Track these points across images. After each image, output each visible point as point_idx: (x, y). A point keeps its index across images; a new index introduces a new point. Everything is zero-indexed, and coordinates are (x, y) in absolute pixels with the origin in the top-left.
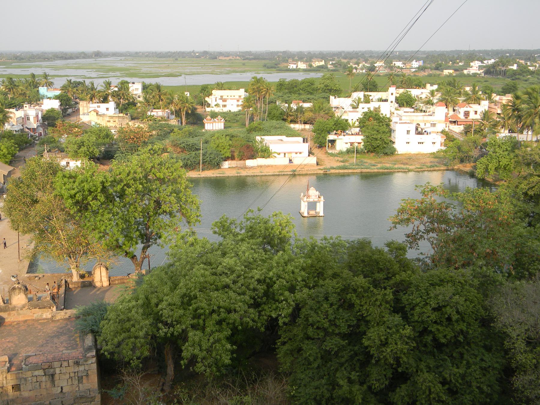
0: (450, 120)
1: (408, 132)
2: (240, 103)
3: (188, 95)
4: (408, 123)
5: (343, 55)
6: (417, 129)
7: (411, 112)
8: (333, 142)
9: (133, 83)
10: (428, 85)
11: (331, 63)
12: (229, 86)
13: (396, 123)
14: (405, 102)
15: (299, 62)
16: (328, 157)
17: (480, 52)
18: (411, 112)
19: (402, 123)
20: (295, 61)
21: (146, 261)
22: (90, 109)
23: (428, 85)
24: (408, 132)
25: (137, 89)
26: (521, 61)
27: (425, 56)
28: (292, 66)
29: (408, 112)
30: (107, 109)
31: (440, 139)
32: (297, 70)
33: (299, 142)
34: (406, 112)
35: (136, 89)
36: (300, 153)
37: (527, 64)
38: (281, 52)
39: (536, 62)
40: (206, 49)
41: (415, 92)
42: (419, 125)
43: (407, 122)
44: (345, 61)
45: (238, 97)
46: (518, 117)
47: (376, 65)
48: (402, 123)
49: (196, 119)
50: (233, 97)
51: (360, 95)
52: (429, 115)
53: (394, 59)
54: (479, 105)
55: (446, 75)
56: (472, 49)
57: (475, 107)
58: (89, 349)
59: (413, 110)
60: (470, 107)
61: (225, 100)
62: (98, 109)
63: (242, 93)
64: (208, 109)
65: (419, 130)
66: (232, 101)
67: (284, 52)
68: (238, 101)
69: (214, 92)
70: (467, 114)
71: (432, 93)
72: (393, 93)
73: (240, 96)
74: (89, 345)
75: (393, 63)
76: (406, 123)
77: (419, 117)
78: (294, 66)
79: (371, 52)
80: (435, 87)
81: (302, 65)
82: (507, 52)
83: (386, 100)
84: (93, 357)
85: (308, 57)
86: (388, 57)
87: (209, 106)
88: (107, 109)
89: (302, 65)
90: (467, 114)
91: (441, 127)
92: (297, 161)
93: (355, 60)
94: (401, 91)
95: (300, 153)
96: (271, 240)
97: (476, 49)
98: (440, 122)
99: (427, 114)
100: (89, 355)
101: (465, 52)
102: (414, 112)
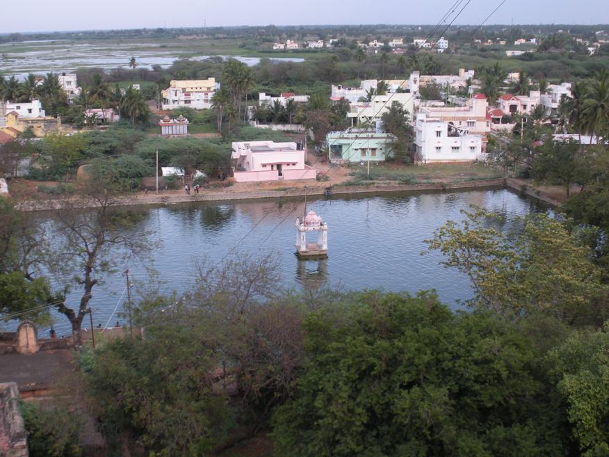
0: (492, 116)
1: (438, 133)
2: (210, 95)
3: (139, 88)
4: (438, 121)
5: (347, 31)
6: (450, 129)
7: (441, 106)
8: (338, 150)
9: (64, 74)
10: (462, 71)
11: (331, 41)
12: (194, 73)
13: (422, 121)
14: (428, 94)
15: (289, 41)
16: (234, 223)
17: (526, 27)
18: (441, 106)
19: (430, 121)
20: (282, 41)
21: (87, 317)
22: (8, 112)
23: (462, 71)
24: (438, 133)
25: (69, 83)
26: (578, 40)
27: (456, 32)
28: (278, 46)
29: (437, 107)
30: (30, 111)
31: (479, 143)
32: (284, 52)
33: (289, 149)
34: (433, 109)
35: (70, 85)
36: (294, 164)
37: (585, 44)
38: (264, 28)
39: (596, 41)
40: (162, 26)
41: (441, 80)
42: (452, 124)
43: (437, 119)
44: (351, 39)
45: (206, 90)
46: (578, 114)
47: (391, 44)
48: (430, 121)
49: (145, 121)
50: (199, 90)
51: (373, 84)
52: (465, 111)
53: (416, 36)
54: (529, 96)
55: (483, 58)
56: (515, 23)
57: (524, 99)
58: (18, 437)
59: (443, 104)
60: (517, 99)
61: (188, 94)
62: (17, 111)
63: (212, 83)
64: (165, 107)
65: (453, 130)
66: (199, 94)
67: (268, 28)
68: (206, 94)
69: (172, 83)
70: (513, 108)
71: (469, 82)
72: (415, 81)
73: (209, 88)
74: (17, 431)
75: (415, 41)
76: (435, 121)
77: (451, 112)
78: (282, 47)
79: (383, 26)
80: (472, 73)
81: (292, 45)
82: (559, 27)
83: (408, 91)
84: (23, 447)
85: (301, 33)
86: (409, 34)
87: (166, 101)
88: (30, 111)
89: (292, 45)
90: (513, 108)
91: (483, 127)
92: (289, 175)
93: (363, 38)
94: (427, 78)
95: (294, 164)
96: (30, 352)
97: (521, 24)
98: (479, 119)
99: (462, 108)
100: (18, 444)
101: (508, 27)
102: (444, 106)
